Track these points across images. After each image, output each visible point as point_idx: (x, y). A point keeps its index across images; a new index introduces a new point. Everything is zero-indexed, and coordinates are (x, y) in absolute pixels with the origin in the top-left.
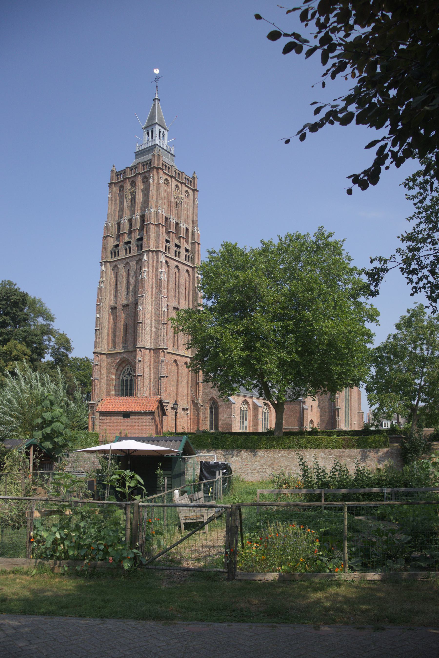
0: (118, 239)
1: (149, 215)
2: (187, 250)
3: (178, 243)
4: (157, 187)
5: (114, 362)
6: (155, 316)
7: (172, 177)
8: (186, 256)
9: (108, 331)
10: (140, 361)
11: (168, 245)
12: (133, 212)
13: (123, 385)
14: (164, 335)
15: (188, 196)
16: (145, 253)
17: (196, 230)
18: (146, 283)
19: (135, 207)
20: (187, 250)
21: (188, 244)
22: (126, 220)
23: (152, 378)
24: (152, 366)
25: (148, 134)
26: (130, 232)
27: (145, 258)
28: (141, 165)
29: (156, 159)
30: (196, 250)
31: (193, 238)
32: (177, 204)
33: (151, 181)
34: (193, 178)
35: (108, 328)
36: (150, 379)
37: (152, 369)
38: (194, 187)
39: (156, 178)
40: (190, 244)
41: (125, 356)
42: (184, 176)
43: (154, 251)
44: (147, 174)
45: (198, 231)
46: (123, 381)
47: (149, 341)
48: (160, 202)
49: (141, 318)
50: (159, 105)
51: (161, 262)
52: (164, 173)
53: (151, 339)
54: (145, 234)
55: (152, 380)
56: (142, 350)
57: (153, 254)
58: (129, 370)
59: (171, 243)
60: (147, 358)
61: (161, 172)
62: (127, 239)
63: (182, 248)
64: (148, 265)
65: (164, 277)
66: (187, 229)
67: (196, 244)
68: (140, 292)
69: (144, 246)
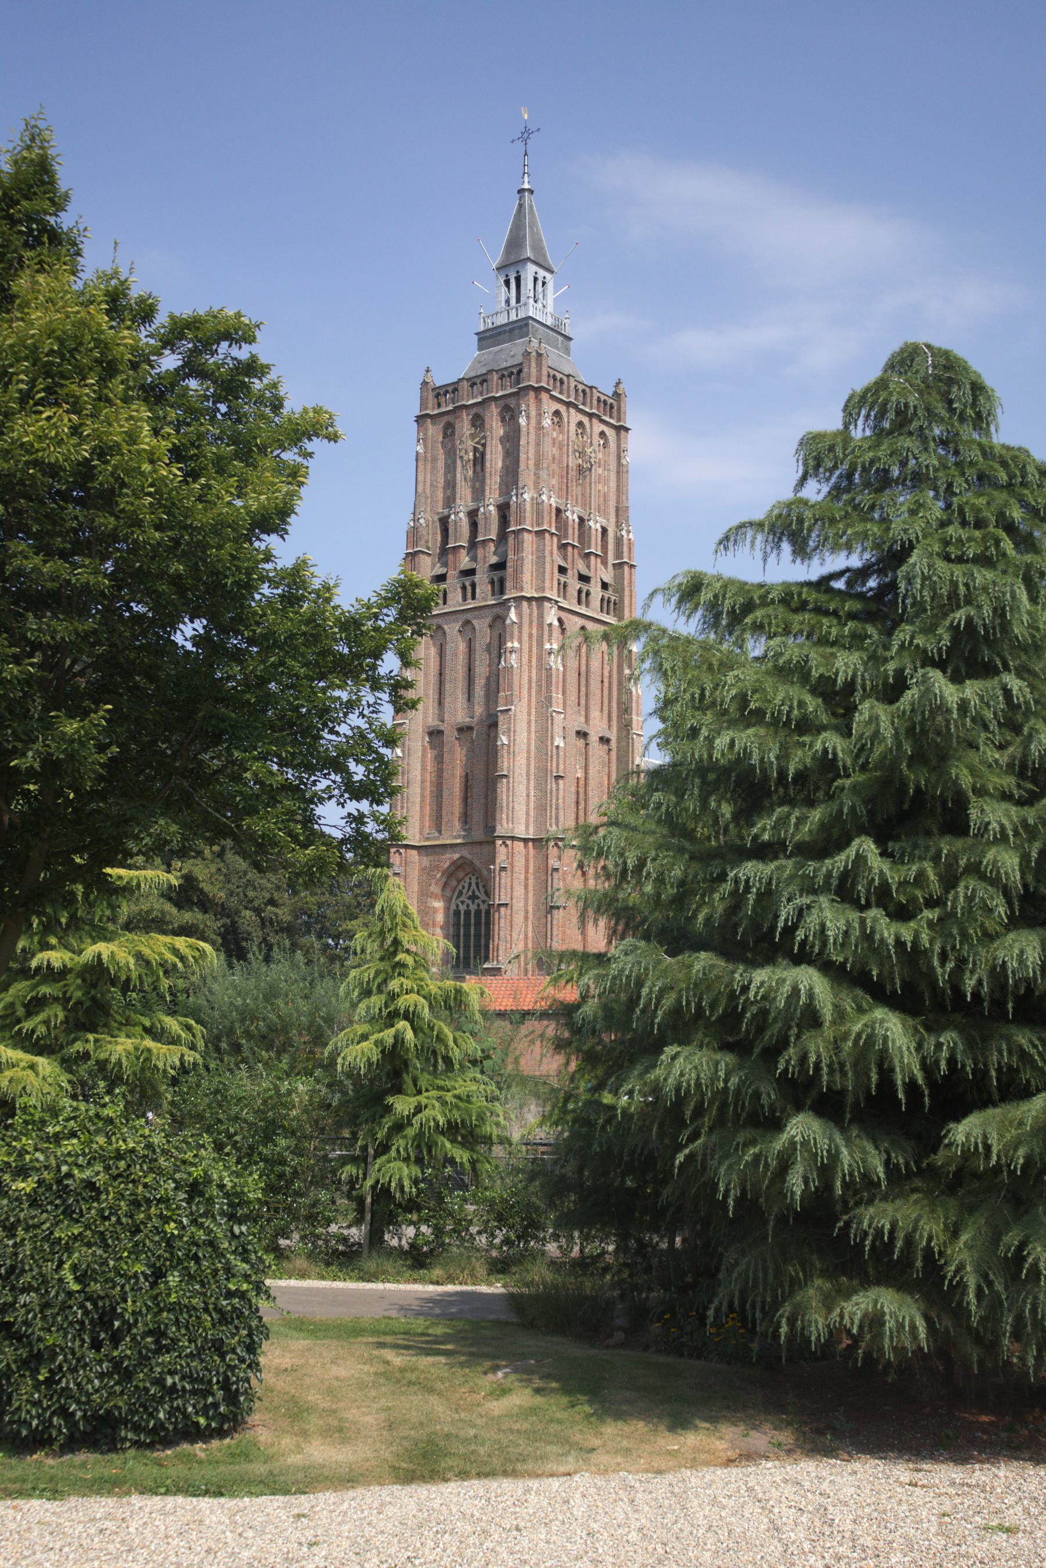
0: (444, 559)
1: (520, 506)
2: (605, 586)
3: (584, 572)
4: (538, 436)
5: (437, 867)
6: (538, 760)
7: (568, 404)
8: (602, 600)
9: (423, 788)
10: (503, 869)
11: (563, 580)
12: (478, 494)
13: (457, 925)
14: (557, 805)
15: (605, 446)
16: (512, 604)
17: (624, 533)
18: (516, 678)
19: (483, 482)
20: (605, 586)
21: (606, 567)
22: (461, 515)
23: (530, 909)
24: (531, 882)
25: (507, 283)
26: (473, 544)
27: (513, 615)
28: (495, 377)
29: (533, 364)
30: (626, 582)
31: (619, 554)
32: (580, 470)
33: (523, 421)
34: (617, 395)
35: (423, 781)
36: (526, 912)
37: (531, 888)
38: (619, 420)
39: (533, 413)
40: (610, 568)
41: (466, 853)
42: (596, 394)
43: (529, 600)
44: (512, 403)
45: (628, 532)
46: (457, 913)
47: (523, 821)
48: (543, 474)
49: (506, 764)
50: (531, 207)
51: (550, 625)
52: (553, 397)
53: (528, 814)
54: (511, 556)
55: (531, 916)
56: (509, 842)
57: (530, 606)
58: (474, 886)
59: (570, 572)
60: (519, 862)
61: (544, 396)
62: (464, 561)
63: (593, 581)
64: (520, 632)
65: (555, 663)
66: (604, 531)
67: (626, 568)
68: (501, 701)
69: (509, 584)
